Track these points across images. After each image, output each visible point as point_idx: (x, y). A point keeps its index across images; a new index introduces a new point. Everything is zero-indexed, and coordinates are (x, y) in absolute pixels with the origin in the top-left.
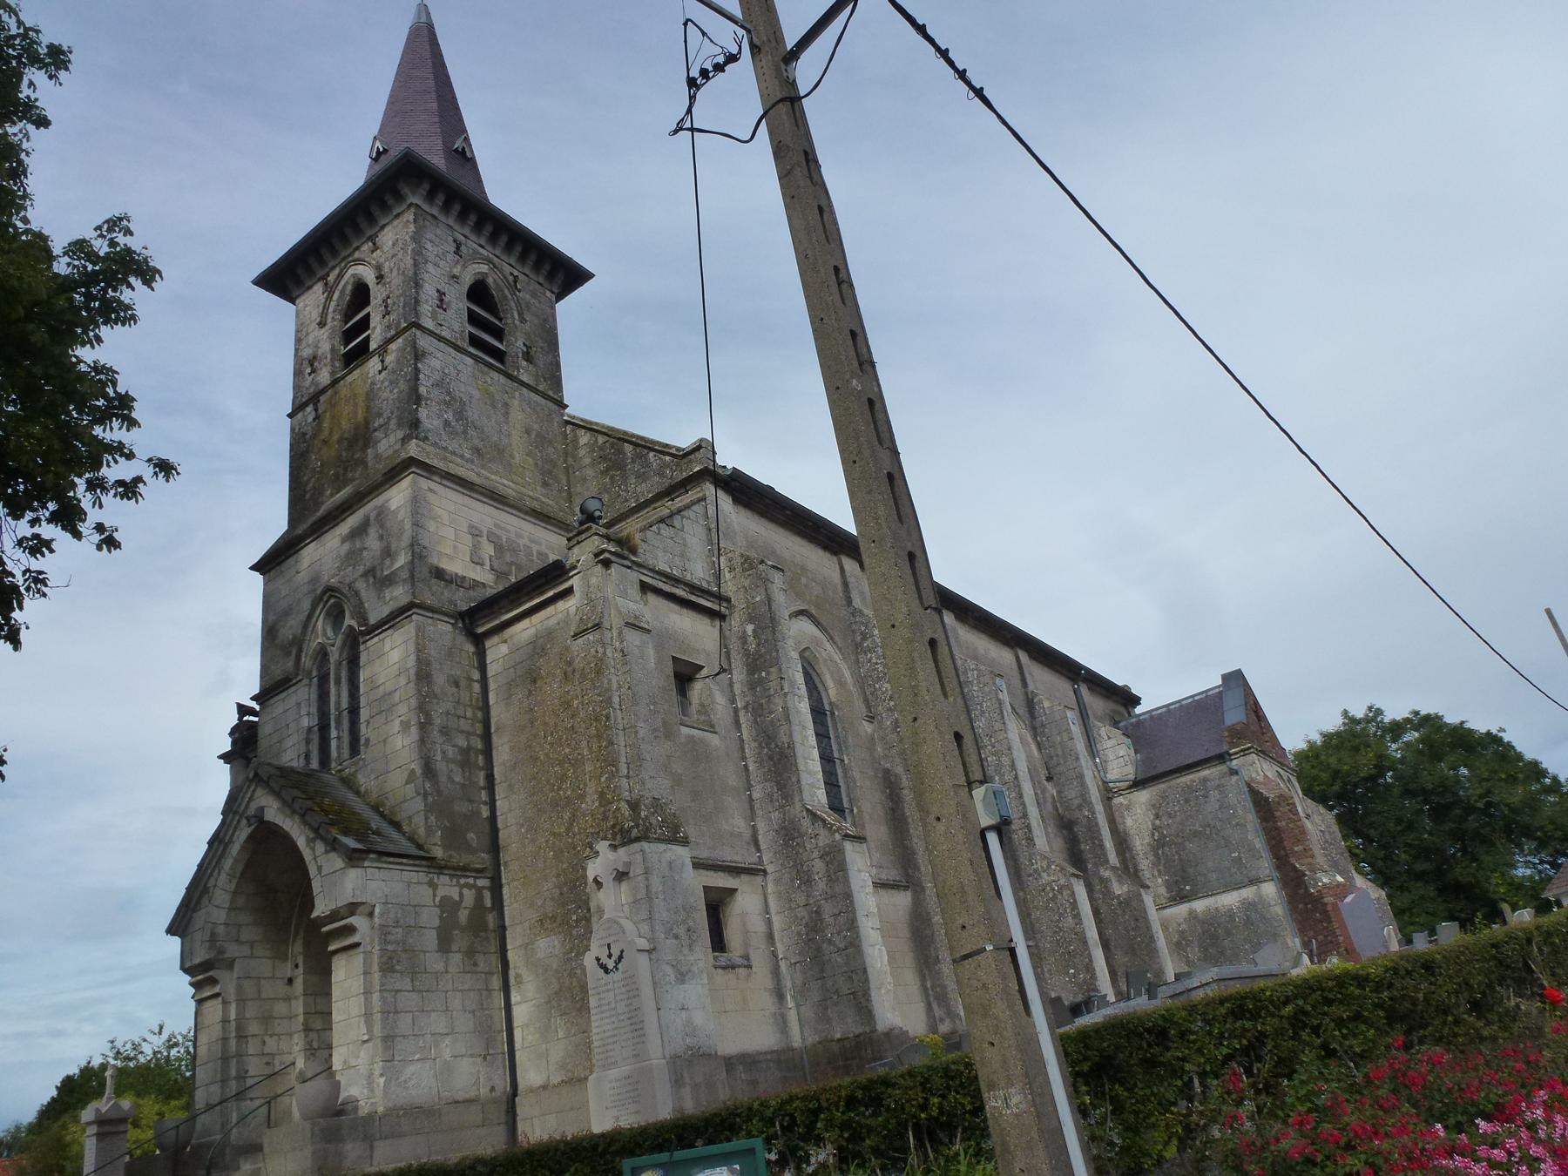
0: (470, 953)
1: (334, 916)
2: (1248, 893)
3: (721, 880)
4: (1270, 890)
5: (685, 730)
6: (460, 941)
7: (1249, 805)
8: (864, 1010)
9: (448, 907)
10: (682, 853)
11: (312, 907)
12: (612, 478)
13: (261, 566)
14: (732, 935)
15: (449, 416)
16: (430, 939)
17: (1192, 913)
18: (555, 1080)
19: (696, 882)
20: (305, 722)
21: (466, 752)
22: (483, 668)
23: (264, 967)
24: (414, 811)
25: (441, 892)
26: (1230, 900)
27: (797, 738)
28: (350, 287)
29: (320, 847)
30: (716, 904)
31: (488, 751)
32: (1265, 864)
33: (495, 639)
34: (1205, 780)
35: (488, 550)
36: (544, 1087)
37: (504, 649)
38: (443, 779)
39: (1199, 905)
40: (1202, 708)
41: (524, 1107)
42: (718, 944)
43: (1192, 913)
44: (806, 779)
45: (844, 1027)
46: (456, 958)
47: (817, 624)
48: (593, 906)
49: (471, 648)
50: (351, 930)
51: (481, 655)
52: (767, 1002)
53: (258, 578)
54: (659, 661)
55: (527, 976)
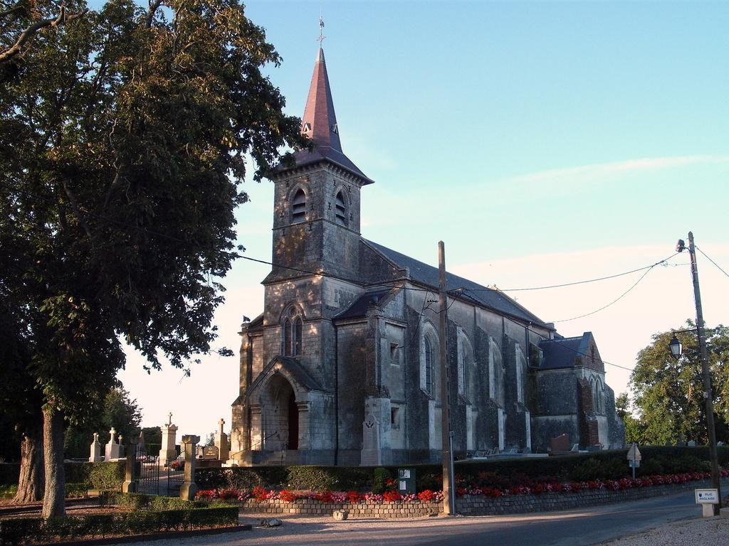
0: (330, 414)
1: (302, 403)
2: (567, 417)
3: (395, 406)
4: (575, 417)
5: (392, 365)
6: (328, 411)
7: (576, 387)
8: (427, 444)
9: (326, 402)
10: (389, 400)
11: (295, 399)
12: (375, 268)
13: (265, 283)
14: (396, 419)
15: (330, 250)
16: (322, 412)
17: (547, 420)
18: (349, 448)
19: (390, 406)
20: (281, 340)
21: (331, 360)
22: (336, 335)
23: (270, 407)
24: (320, 376)
25: (325, 398)
26: (562, 418)
27: (421, 369)
28: (296, 191)
29: (298, 385)
30: (394, 411)
31: (336, 360)
32: (575, 409)
33: (341, 328)
34: (563, 374)
35: (339, 296)
36: (346, 449)
37: (343, 332)
38: (326, 368)
39: (550, 418)
40: (574, 344)
41: (340, 453)
42: (393, 422)
43: (547, 420)
44: (421, 381)
45: (421, 446)
46: (327, 415)
47: (432, 324)
48: (366, 410)
49: (333, 329)
50: (307, 407)
51: (336, 331)
52: (403, 437)
53: (263, 287)
54: (388, 345)
55: (343, 422)
